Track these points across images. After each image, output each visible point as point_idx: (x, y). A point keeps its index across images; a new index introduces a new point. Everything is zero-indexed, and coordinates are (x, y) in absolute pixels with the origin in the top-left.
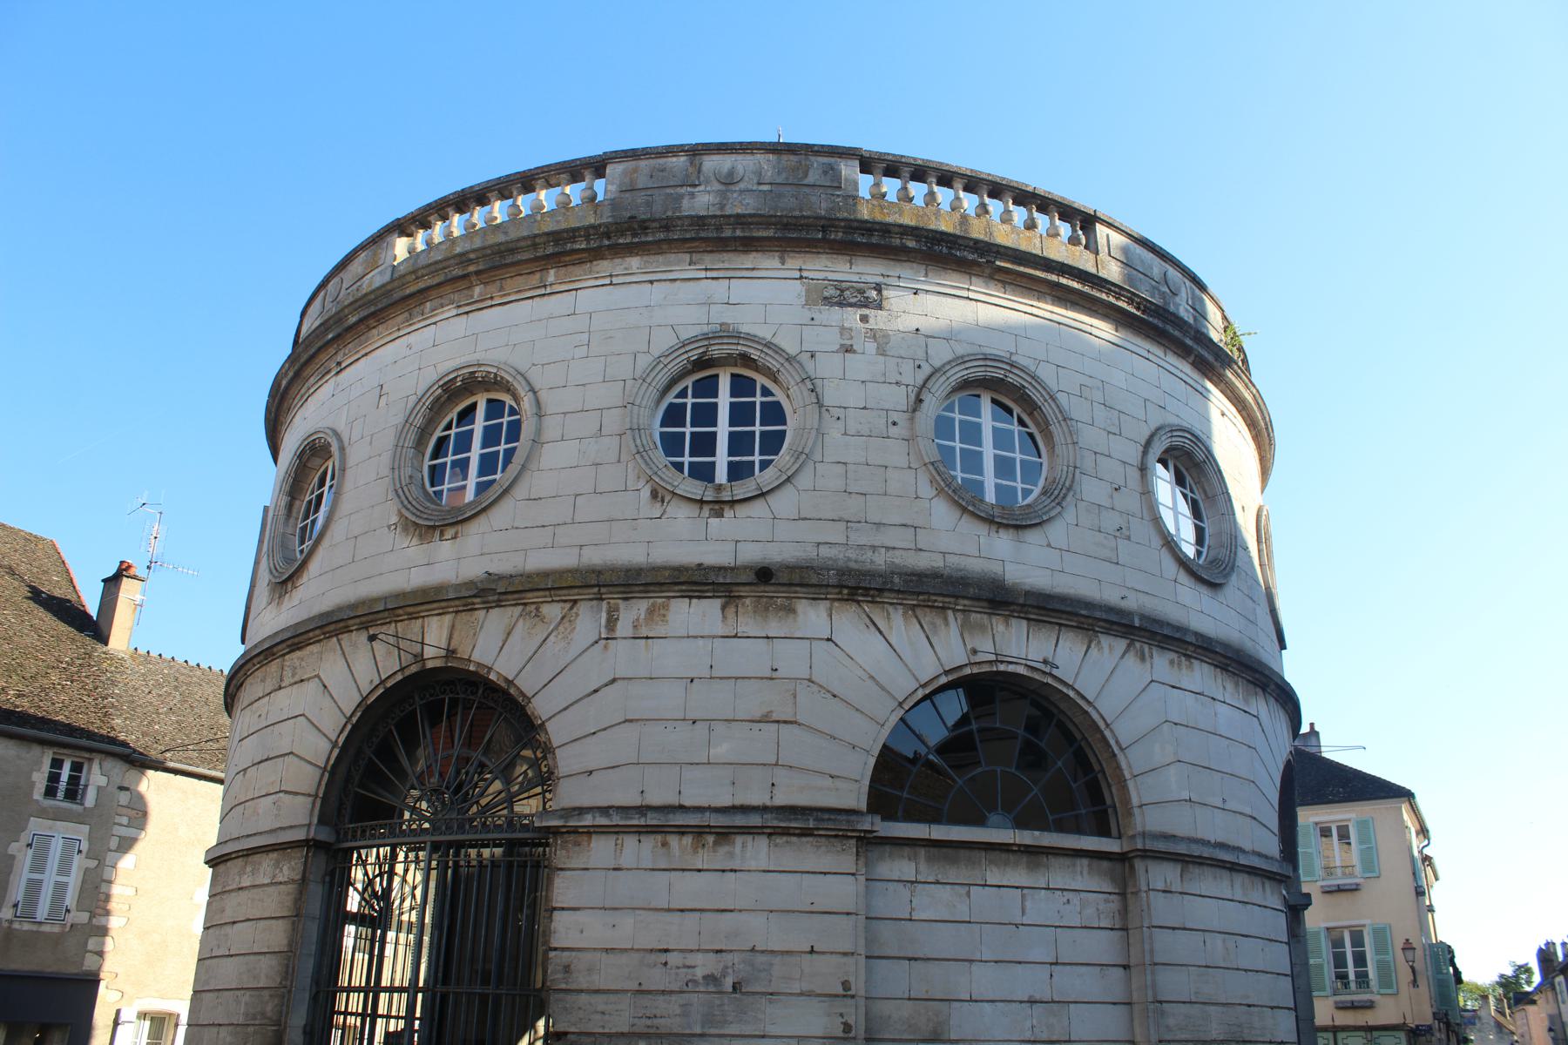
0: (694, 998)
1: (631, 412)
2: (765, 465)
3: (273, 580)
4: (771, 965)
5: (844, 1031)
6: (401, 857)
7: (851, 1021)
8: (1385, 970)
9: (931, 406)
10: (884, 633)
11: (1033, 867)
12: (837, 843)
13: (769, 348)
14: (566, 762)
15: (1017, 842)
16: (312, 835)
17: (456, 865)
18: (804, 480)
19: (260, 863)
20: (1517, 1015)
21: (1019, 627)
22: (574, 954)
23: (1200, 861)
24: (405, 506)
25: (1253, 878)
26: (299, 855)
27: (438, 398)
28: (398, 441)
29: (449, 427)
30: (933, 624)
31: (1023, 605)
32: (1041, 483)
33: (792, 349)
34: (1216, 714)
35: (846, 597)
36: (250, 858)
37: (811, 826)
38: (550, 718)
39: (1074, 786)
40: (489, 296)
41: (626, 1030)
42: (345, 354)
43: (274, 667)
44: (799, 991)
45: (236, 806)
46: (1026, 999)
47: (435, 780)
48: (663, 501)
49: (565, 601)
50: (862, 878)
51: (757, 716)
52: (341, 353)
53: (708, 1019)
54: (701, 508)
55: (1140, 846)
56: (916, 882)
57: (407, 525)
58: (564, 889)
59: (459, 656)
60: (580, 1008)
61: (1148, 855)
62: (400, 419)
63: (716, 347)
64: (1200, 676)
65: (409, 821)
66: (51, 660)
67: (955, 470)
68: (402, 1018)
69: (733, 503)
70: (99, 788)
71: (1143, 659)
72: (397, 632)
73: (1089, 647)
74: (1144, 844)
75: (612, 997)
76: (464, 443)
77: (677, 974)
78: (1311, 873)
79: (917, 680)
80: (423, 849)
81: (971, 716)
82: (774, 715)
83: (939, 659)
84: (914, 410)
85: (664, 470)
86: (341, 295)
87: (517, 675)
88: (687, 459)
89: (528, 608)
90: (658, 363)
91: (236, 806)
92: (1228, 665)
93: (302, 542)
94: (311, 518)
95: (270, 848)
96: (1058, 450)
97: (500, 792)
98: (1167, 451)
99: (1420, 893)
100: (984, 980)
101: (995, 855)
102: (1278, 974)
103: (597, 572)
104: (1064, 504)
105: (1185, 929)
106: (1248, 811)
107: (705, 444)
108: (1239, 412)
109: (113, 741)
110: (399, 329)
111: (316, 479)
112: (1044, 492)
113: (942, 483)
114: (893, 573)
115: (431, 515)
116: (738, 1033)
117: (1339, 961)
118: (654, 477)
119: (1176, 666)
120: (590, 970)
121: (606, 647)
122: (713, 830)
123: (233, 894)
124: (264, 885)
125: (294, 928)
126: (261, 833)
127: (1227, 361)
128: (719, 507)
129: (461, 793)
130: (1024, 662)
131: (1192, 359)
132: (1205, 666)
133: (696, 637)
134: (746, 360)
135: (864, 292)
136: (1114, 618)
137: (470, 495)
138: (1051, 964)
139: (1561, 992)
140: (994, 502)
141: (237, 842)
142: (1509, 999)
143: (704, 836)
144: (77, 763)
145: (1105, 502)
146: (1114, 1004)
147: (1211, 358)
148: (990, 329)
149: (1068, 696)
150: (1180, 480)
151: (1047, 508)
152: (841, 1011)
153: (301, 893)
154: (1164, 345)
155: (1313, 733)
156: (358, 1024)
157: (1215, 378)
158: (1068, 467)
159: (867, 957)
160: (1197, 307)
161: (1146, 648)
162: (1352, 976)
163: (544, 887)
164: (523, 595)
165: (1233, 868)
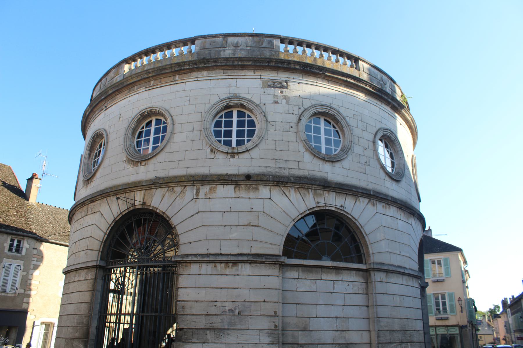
0: (225, 317)
1: (204, 123)
2: (248, 141)
3: (85, 179)
4: (251, 306)
5: (275, 328)
6: (128, 271)
7: (277, 324)
8: (452, 307)
9: (304, 121)
11: (337, 274)
12: (273, 266)
13: (250, 102)
14: (183, 239)
15: (332, 265)
16: (98, 264)
18: (261, 146)
19: (81, 273)
20: (495, 322)
21: (333, 195)
22: (185, 302)
23: (392, 272)
24: (128, 155)
25: (409, 277)
26: (94, 270)
27: (139, 119)
28: (126, 133)
29: (143, 128)
30: (304, 194)
31: (334, 188)
32: (340, 147)
33: (258, 102)
34: (398, 223)
35: (275, 185)
37: (264, 260)
38: (177, 225)
39: (351, 247)
41: (203, 327)
42: (108, 104)
43: (85, 208)
44: (260, 314)
47: (139, 245)
48: (214, 153)
49: (182, 186)
50: (281, 278)
52: (106, 104)
53: (230, 324)
54: (227, 155)
55: (372, 267)
56: (299, 279)
57: (129, 161)
58: (182, 281)
60: (187, 320)
61: (375, 270)
62: (127, 125)
63: (232, 101)
64: (393, 211)
65: (130, 259)
66: (10, 206)
67: (312, 142)
68: (129, 324)
69: (238, 153)
70: (27, 249)
71: (374, 205)
73: (356, 201)
74: (374, 266)
75: (198, 317)
76: (148, 133)
77: (219, 309)
78: (428, 276)
79: (299, 212)
81: (317, 224)
82: (252, 224)
83: (306, 205)
84: (298, 123)
85: (215, 142)
88: (222, 139)
89: (170, 188)
90: (213, 107)
93: (94, 166)
94: (97, 159)
95: (84, 268)
96: (346, 136)
97: (161, 249)
98: (382, 136)
99: (464, 282)
100: (321, 311)
101: (325, 270)
102: (417, 309)
103: (193, 176)
104: (348, 154)
106: (408, 255)
107: (228, 134)
108: (406, 123)
109: (31, 233)
110: (126, 95)
111: (98, 146)
112: (341, 150)
113: (307, 147)
114: (291, 177)
116: (239, 328)
117: (437, 304)
118: (211, 145)
120: (191, 308)
121: (196, 201)
122: (231, 262)
123: (72, 283)
125: (93, 294)
127: (403, 107)
128: (233, 155)
129: (148, 250)
130: (334, 206)
131: (390, 106)
132: (394, 208)
133: (225, 198)
134: (242, 106)
136: (364, 192)
137: (150, 151)
138: (343, 305)
139: (509, 314)
140: (325, 153)
141: (73, 266)
142: (492, 316)
143: (228, 263)
145: (362, 153)
146: (364, 318)
147: (397, 106)
148: (324, 95)
149: (349, 217)
150: (386, 146)
151: (342, 155)
153: (95, 283)
154: (381, 101)
155: (430, 230)
156: (114, 326)
157: (398, 112)
158: (349, 141)
159: (282, 303)
160: (393, 89)
162: (441, 309)
163: (176, 281)
164: (168, 184)
165: (403, 274)
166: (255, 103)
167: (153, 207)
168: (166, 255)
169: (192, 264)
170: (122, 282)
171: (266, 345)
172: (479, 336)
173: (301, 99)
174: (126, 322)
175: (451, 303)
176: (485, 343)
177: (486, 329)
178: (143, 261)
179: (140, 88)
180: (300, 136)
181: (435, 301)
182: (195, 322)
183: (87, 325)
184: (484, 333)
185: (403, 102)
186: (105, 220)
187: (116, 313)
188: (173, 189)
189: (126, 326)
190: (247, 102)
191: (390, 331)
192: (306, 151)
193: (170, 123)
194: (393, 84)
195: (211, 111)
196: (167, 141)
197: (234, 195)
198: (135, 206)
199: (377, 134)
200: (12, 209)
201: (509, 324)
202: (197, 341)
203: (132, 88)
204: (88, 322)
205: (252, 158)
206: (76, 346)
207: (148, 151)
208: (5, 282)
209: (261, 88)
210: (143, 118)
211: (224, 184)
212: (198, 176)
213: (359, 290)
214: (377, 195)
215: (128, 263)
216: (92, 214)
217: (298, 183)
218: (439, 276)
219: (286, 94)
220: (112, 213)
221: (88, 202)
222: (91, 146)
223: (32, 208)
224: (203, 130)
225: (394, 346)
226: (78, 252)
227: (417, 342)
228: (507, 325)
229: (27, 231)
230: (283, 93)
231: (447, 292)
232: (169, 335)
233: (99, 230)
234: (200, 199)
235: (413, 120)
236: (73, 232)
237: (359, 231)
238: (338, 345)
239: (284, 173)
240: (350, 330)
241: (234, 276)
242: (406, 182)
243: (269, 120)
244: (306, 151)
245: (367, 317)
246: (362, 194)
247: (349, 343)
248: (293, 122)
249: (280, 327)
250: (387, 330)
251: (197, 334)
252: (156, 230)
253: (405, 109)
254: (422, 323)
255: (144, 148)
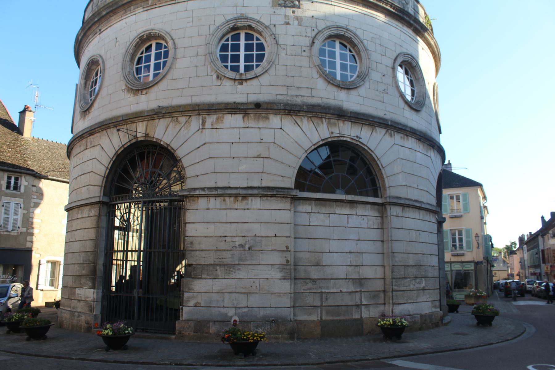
0: (235, 252)
1: (209, 47)
2: (257, 66)
3: (81, 110)
4: (262, 241)
5: (287, 263)
6: (133, 206)
7: (289, 259)
8: (468, 243)
9: (318, 44)
10: (300, 126)
11: (351, 208)
12: (284, 200)
13: (259, 23)
14: (189, 172)
15: (346, 199)
16: (101, 200)
17: (152, 209)
18: (272, 72)
19: (84, 210)
20: (510, 258)
21: (348, 124)
22: (194, 238)
23: (408, 206)
24: (127, 83)
25: (427, 212)
26: (97, 207)
27: (138, 43)
28: (124, 59)
29: (142, 53)
30: (318, 123)
31: (350, 117)
32: (357, 73)
33: (267, 23)
34: (416, 156)
35: (287, 113)
36: (80, 208)
37: (275, 194)
38: (183, 157)
39: (366, 180)
40: (155, 4)
41: (212, 263)
42: (102, 26)
43: (84, 141)
44: (271, 249)
45: (74, 190)
46: (348, 252)
47: (143, 180)
48: (221, 79)
49: (187, 116)
50: (293, 211)
51: (256, 155)
52: (101, 26)
53: (240, 259)
54: (235, 82)
55: (388, 201)
56: (311, 213)
57: (128, 89)
58: (189, 216)
59: (150, 136)
60: (196, 256)
61: (391, 204)
62: (124, 50)
63: (239, 23)
64: (411, 142)
65: (135, 194)
66: (3, 141)
67: (326, 68)
68: (136, 261)
69: (246, 80)
70: (25, 186)
71: (391, 136)
72: (127, 128)
73: (372, 132)
74: (390, 200)
75: (208, 252)
76: (148, 59)
77: (229, 244)
78: (446, 211)
79: (312, 143)
80: (140, 204)
81: (331, 156)
82: (262, 155)
83: (320, 136)
84: (312, 46)
85: (221, 68)
86: (99, 4)
87: (171, 142)
88: (229, 64)
89: (174, 119)
90: (218, 29)
91: (74, 190)
92: (421, 139)
93: (91, 96)
94: (94, 88)
95: (87, 205)
96: (363, 61)
97: (166, 183)
98: (402, 62)
99: (482, 218)
100: (334, 246)
101: (338, 203)
102: (433, 244)
103: (198, 105)
104: (365, 81)
105: (403, 229)
106: (426, 189)
107: (236, 59)
108: (429, 48)
109: (29, 169)
110: (122, 17)
111: (94, 74)
112: (358, 76)
113: (321, 73)
114: (303, 105)
115: (137, 85)
116: (250, 263)
117: (454, 240)
118: (217, 71)
119: (403, 138)
120: (199, 243)
121: (202, 132)
122: (241, 195)
123: (75, 221)
124: (86, 217)
125: (97, 232)
126: (83, 200)
127: (426, 30)
128: (241, 81)
129: (153, 184)
130: (349, 137)
131: (412, 28)
132: (413, 139)
133: (233, 128)
134: (250, 27)
135: (293, 2)
136: (381, 122)
137: (151, 78)
138: (357, 240)
139: (525, 250)
140: (340, 80)
141: (75, 203)
142: (508, 253)
143: (238, 197)
144: (17, 177)
145: (380, 80)
146: (378, 253)
147: (419, 28)
148: (339, 16)
149: (364, 149)
150: (406, 73)
151: (359, 82)
152: (286, 256)
153: (99, 219)
154: (403, 23)
155: (449, 164)
156: (121, 263)
157: (421, 36)
158: (367, 67)
159: (294, 238)
160: (415, 9)
161: (393, 132)
162: (458, 245)
163: (183, 216)
164: (172, 114)
165: (420, 208)
166: (264, 24)
167: (157, 139)
168: (172, 190)
169: (200, 198)
170: (127, 218)
171: (278, 280)
172: (493, 272)
173: (314, 20)
174: (133, 260)
175: (468, 239)
176: (498, 279)
177: (501, 265)
178: (148, 196)
179: (137, 8)
180: (313, 61)
181: (451, 237)
182: (205, 257)
183: (94, 263)
184: (499, 269)
185: (427, 24)
186: (106, 154)
187: (122, 250)
188: (177, 119)
189: (134, 264)
190: (255, 23)
191: (405, 266)
192: (320, 77)
193: (171, 48)
194: (416, 3)
195: (216, 33)
196: (169, 67)
197: (242, 125)
198: (137, 138)
199: (397, 60)
200: (6, 145)
201: (524, 260)
202: (207, 277)
203: (127, 8)
204: (95, 259)
205: (261, 85)
206: (84, 283)
207: (149, 78)
208: (6, 220)
209: (271, 7)
210: (142, 43)
211: (232, 113)
212: (203, 104)
213: (374, 225)
214: (395, 126)
215: (133, 198)
216: (92, 148)
217: (311, 112)
218: (457, 212)
219: (298, 14)
220: (113, 146)
221: (87, 135)
222: (87, 74)
223: (27, 143)
224: (208, 54)
225: (408, 281)
226: (80, 188)
227: (431, 277)
228: (522, 262)
229: (24, 168)
230: (294, 13)
231: (464, 228)
232: (179, 272)
233: (100, 164)
234: (207, 130)
235: (436, 44)
236: (73, 167)
237: (375, 163)
238: (351, 280)
239: (296, 101)
240: (364, 265)
241: (243, 210)
242: (426, 112)
243: (279, 44)
244: (320, 77)
245: (382, 252)
246: (379, 124)
247: (362, 278)
248: (306, 45)
249: (292, 262)
250: (402, 266)
251: (207, 270)
252: (160, 163)
253: (428, 32)
254: (438, 259)
255: (145, 75)
